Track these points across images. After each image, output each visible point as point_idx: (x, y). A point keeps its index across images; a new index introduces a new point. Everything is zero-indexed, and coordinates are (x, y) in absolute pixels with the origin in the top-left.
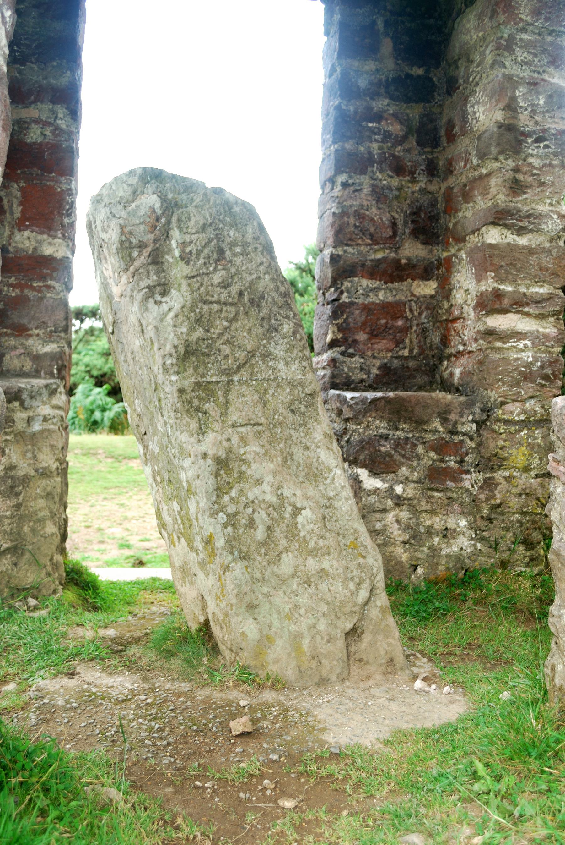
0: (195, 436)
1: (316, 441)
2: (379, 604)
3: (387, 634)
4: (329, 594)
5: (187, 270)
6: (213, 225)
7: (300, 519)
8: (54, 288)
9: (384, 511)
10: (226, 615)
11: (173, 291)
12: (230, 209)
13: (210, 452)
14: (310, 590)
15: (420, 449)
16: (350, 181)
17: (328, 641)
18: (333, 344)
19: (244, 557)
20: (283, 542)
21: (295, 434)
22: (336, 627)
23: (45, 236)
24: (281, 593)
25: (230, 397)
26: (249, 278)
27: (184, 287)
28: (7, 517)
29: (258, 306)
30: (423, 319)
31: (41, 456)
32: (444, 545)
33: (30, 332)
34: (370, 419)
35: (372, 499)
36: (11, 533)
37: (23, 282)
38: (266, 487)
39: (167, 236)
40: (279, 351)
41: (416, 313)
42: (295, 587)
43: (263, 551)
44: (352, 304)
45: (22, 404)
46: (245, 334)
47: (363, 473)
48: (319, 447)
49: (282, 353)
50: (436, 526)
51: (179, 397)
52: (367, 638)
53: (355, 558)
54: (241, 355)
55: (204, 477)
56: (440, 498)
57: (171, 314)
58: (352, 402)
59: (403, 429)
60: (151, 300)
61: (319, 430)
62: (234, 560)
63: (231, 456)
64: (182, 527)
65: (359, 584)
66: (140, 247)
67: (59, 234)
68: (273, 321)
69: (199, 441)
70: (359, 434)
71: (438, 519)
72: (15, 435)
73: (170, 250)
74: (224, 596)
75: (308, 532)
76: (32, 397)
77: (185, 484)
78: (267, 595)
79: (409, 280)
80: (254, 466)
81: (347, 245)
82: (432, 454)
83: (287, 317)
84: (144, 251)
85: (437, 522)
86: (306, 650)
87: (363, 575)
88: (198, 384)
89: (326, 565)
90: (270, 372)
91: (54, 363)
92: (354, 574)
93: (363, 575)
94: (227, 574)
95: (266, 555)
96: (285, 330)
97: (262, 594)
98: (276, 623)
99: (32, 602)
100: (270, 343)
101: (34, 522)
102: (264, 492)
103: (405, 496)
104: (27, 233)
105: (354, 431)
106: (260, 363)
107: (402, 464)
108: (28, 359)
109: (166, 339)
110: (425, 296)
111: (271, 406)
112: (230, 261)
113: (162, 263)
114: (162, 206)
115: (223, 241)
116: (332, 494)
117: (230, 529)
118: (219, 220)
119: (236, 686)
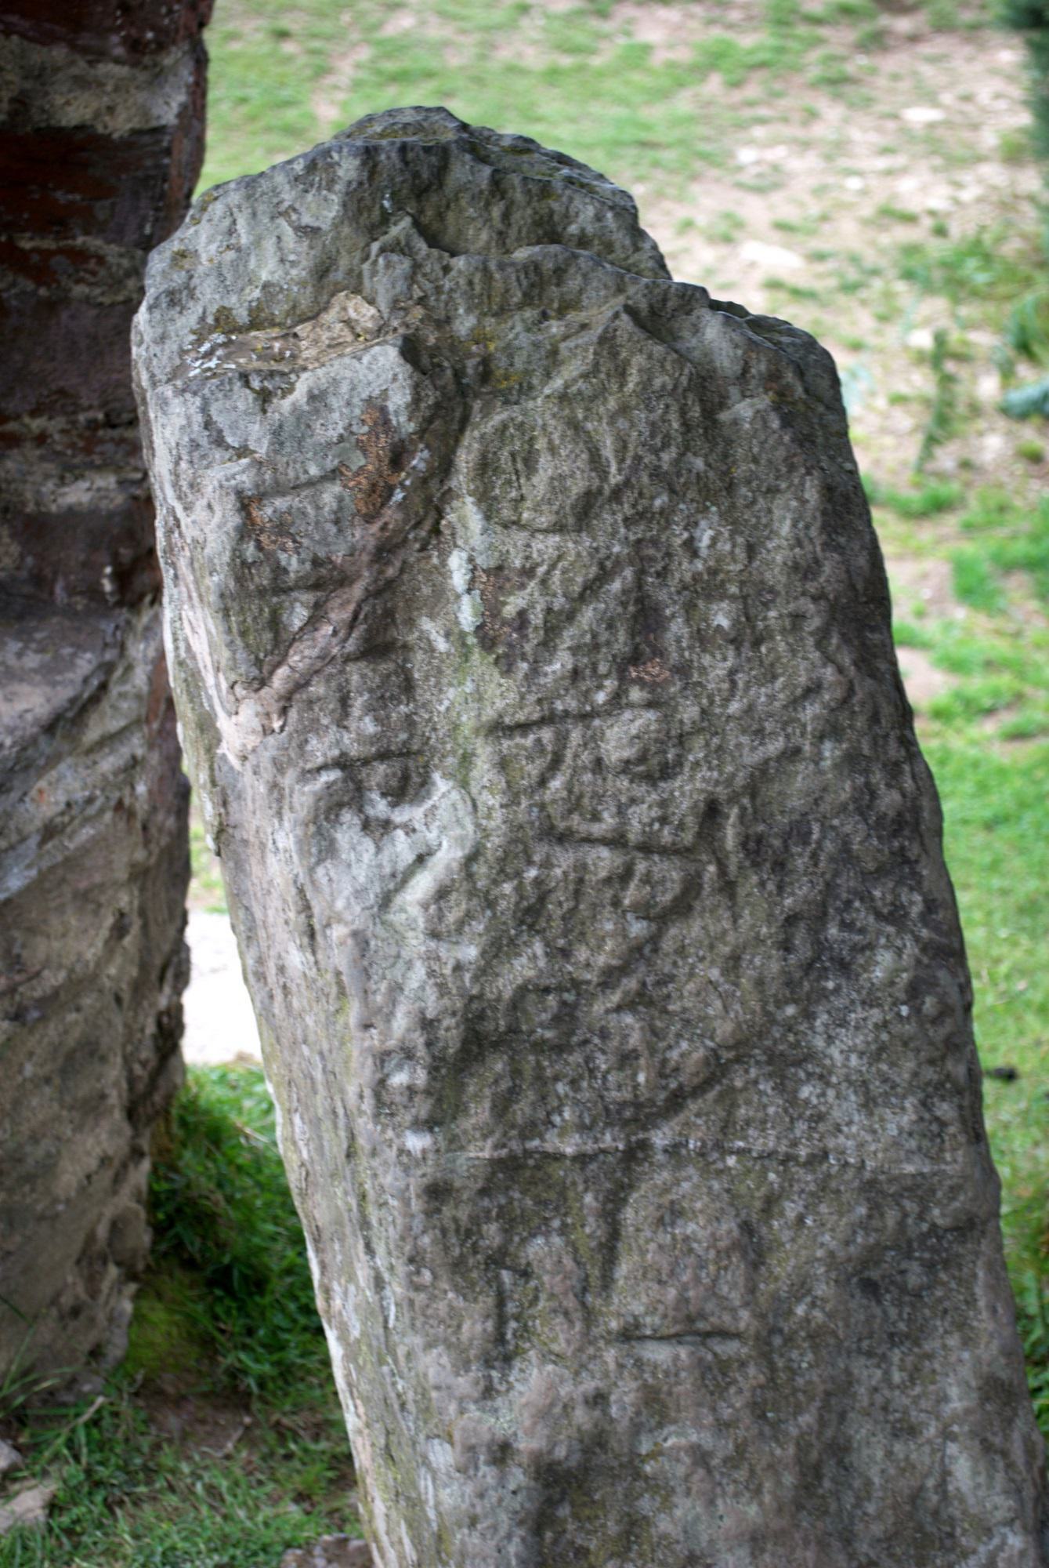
5: (501, 694)
6: (629, 497)
8: (101, 260)
11: (441, 785)
12: (709, 414)
13: (525, 1445)
21: (867, 1373)
23: (59, 53)
25: (629, 1215)
26: (752, 758)
27: (483, 770)
29: (780, 866)
33: (12, 426)
39: (436, 531)
40: (843, 1051)
46: (715, 974)
49: (854, 1060)
51: (428, 1214)
54: (688, 1054)
55: (495, 1528)
57: (423, 885)
61: (965, 1372)
66: (317, 586)
67: (116, 45)
68: (833, 931)
83: (896, 916)
84: (335, 603)
90: (801, 1127)
91: (103, 556)
96: (879, 974)
100: (809, 1016)
106: (765, 1086)
109: (397, 988)
111: (783, 1268)
112: (683, 670)
113: (406, 647)
114: (417, 400)
118: (656, 474)
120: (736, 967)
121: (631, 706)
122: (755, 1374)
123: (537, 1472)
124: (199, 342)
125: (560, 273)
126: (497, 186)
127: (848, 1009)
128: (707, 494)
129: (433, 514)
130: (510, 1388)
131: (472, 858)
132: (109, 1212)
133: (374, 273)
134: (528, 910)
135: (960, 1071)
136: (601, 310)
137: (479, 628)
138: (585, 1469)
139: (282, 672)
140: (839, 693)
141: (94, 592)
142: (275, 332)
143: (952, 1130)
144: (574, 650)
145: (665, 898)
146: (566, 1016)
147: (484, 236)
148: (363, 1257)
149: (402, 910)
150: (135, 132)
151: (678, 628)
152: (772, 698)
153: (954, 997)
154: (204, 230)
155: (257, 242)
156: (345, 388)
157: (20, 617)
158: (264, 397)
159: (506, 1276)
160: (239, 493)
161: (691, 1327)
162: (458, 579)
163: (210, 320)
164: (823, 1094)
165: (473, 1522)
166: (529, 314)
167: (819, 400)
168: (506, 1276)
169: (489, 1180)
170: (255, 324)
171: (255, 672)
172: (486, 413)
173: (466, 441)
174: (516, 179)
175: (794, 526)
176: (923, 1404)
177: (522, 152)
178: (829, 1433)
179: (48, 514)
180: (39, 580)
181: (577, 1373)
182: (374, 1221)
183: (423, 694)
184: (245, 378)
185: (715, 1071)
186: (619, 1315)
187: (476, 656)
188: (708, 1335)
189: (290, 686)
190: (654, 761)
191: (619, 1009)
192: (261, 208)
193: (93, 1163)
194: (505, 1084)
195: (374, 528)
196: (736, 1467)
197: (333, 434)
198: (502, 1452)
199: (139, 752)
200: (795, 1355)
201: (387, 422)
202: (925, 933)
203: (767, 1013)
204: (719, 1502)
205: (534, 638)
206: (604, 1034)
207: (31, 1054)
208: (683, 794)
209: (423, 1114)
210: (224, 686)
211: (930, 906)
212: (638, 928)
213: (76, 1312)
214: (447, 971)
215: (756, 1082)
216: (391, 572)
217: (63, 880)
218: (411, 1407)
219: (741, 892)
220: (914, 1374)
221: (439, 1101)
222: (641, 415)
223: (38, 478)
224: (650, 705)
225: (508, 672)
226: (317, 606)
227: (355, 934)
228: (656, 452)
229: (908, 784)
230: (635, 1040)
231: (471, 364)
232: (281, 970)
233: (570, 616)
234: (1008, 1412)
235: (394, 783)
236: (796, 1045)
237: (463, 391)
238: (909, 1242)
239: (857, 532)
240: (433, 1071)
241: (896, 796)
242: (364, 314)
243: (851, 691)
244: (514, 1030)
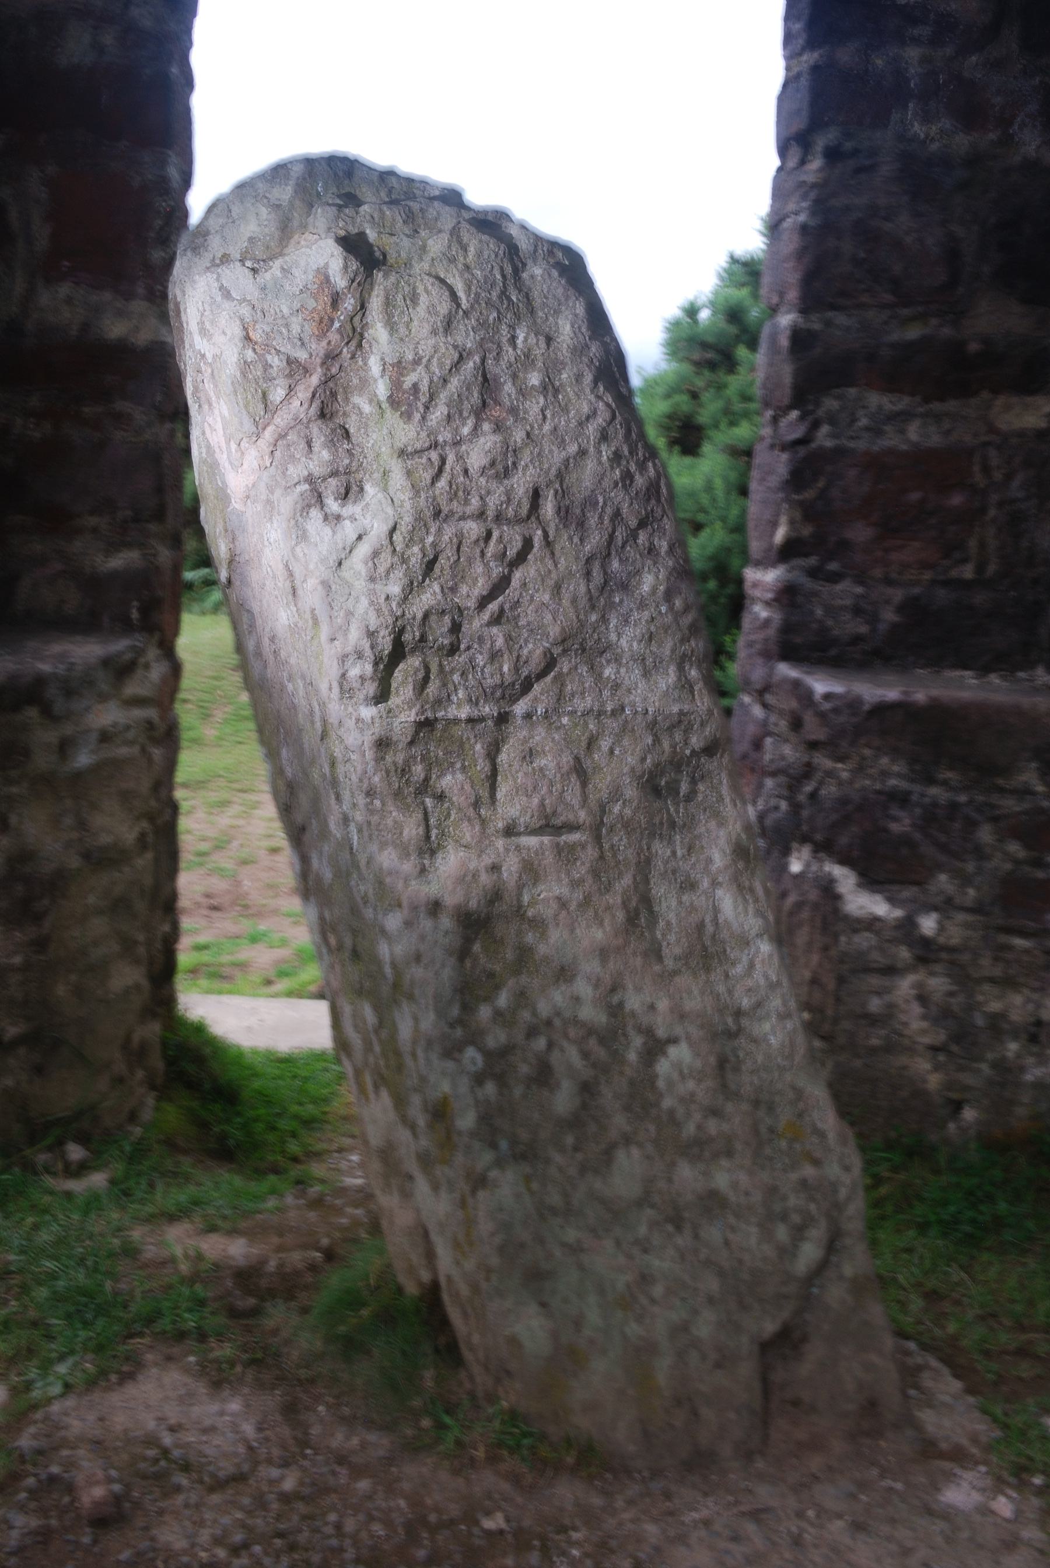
2: (848, 1270)
5: (407, 433)
6: (474, 315)
7: (663, 1067)
9: (891, 971)
10: (475, 1289)
11: (370, 489)
12: (516, 272)
14: (679, 1241)
15: (985, 834)
16: (848, 145)
17: (718, 1365)
18: (787, 552)
19: (525, 1154)
20: (620, 1122)
21: (659, 848)
23: (107, 296)
24: (608, 1244)
25: (503, 758)
27: (398, 479)
29: (581, 524)
30: (1016, 489)
31: (99, 821)
32: (1030, 1060)
34: (867, 752)
35: (864, 940)
38: (583, 988)
40: (627, 640)
41: (998, 476)
42: (643, 1230)
43: (570, 1140)
44: (839, 452)
45: (47, 712)
46: (546, 597)
47: (844, 878)
50: (1015, 1016)
52: (815, 1352)
54: (534, 651)
56: (1027, 951)
57: (364, 549)
58: (827, 706)
59: (945, 783)
60: (315, 513)
62: (499, 1163)
64: (382, 1063)
67: (141, 290)
70: (841, 783)
71: (1018, 999)
73: (365, 383)
77: (388, 970)
78: (575, 1249)
79: (985, 395)
80: (555, 935)
81: (833, 307)
82: (1014, 848)
84: (300, 388)
85: (1017, 1005)
87: (812, 1207)
88: (425, 725)
89: (721, 1180)
90: (606, 693)
93: (812, 1207)
95: (576, 1149)
96: (646, 588)
98: (594, 1317)
99: (75, 1152)
100: (604, 619)
103: (942, 940)
104: (64, 289)
105: (830, 774)
107: (940, 867)
109: (350, 614)
110: (1021, 434)
111: (601, 784)
112: (513, 411)
114: (346, 267)
115: (498, 358)
116: (746, 1003)
117: (490, 1088)
119: (493, 1459)
122: (591, 853)
123: (459, 916)
129: (357, 336)
139: (270, 429)
145: (511, 553)
146: (456, 628)
151: (508, 388)
152: (568, 421)
159: (429, 802)
161: (548, 825)
164: (618, 672)
168: (429, 802)
175: (572, 326)
181: (479, 856)
185: (550, 663)
187: (388, 412)
189: (276, 436)
198: (435, 907)
204: (578, 931)
208: (519, 485)
214: (382, 600)
215: (576, 668)
219: (557, 547)
220: (690, 849)
230: (500, 642)
235: (342, 491)
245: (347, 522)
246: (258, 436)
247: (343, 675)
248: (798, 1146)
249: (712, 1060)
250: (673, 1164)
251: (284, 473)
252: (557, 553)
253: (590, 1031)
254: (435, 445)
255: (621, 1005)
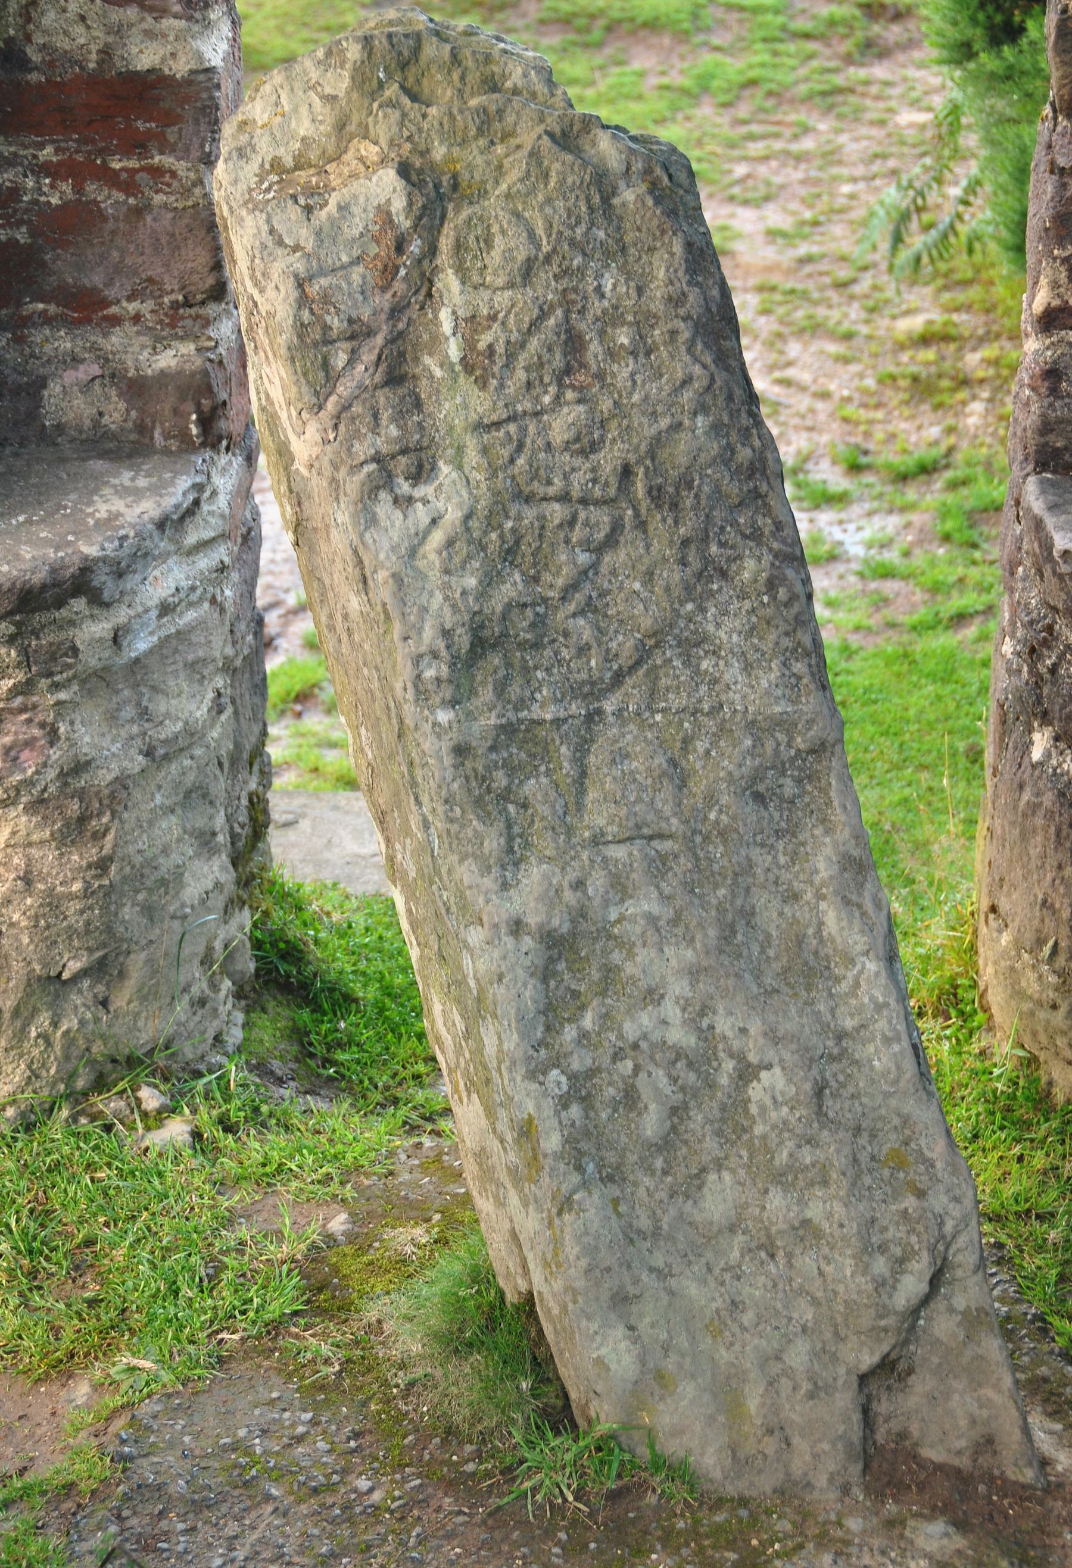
0: (496, 871)
1: (817, 880)
2: (960, 1302)
3: (976, 1374)
4: (818, 1282)
5: (481, 403)
6: (556, 260)
7: (755, 1092)
8: (174, 174)
10: (564, 1308)
11: (444, 469)
12: (606, 200)
13: (532, 920)
17: (811, 1396)
19: (612, 1177)
20: (711, 1144)
21: (762, 859)
22: (834, 1358)
27: (472, 456)
28: (71, 897)
29: (674, 506)
31: (161, 706)
33: (114, 310)
36: (88, 932)
37: (80, 158)
38: (671, 1010)
39: (429, 295)
40: (727, 632)
42: (736, 1254)
43: (659, 1163)
46: (637, 586)
48: (823, 897)
49: (735, 638)
51: (455, 767)
52: (921, 1384)
53: (896, 1196)
54: (624, 644)
57: (437, 537)
61: (828, 850)
62: (585, 1185)
63: (584, 926)
65: (902, 1261)
66: (352, 338)
68: (714, 549)
69: (505, 886)
72: (83, 682)
73: (436, 341)
74: (559, 1265)
75: (774, 1127)
76: (120, 575)
77: (472, 983)
78: (662, 1274)
80: (642, 955)
83: (755, 536)
84: (365, 349)
86: (753, 1410)
88: (508, 730)
89: (814, 1211)
91: (190, 406)
92: (890, 1234)
93: (914, 1239)
94: (566, 1217)
95: (665, 1173)
96: (746, 575)
97: (651, 1270)
99: (151, 1098)
100: (703, 610)
101: (150, 890)
102: (665, 1022)
108: (113, 392)
111: (698, 787)
112: (600, 376)
114: (410, 204)
115: (582, 312)
116: (849, 1023)
117: (575, 1111)
118: (572, 243)
120: (651, 580)
121: (567, 403)
124: (261, 182)
125: (500, 112)
126: (455, 57)
127: (728, 603)
128: (608, 254)
130: (519, 882)
131: (468, 517)
132: (222, 935)
133: (376, 123)
134: (509, 551)
135: (807, 640)
136: (528, 135)
137: (463, 359)
138: (573, 934)
139: (333, 399)
140: (705, 382)
141: (184, 436)
142: (312, 171)
143: (805, 681)
144: (527, 369)
145: (600, 536)
146: (539, 623)
147: (449, 93)
148: (414, 808)
149: (425, 557)
150: (192, 72)
151: (595, 347)
152: (660, 389)
153: (799, 588)
154: (259, 104)
155: (295, 110)
156: (362, 200)
157: (130, 456)
158: (309, 210)
159: (511, 808)
160: (296, 276)
162: (447, 327)
163: (267, 166)
165: (500, 978)
166: (482, 142)
167: (680, 186)
168: (511, 808)
169: (495, 740)
170: (298, 167)
171: (314, 400)
172: (457, 210)
173: (445, 231)
174: (467, 52)
176: (801, 877)
177: (471, 34)
178: (739, 902)
179: (146, 377)
180: (143, 429)
182: (420, 780)
183: (428, 408)
184: (294, 198)
186: (589, 827)
187: (462, 379)
188: (651, 838)
190: (585, 441)
191: (574, 615)
192: (296, 85)
193: (210, 886)
194: (502, 673)
195: (388, 296)
196: (676, 926)
197: (356, 233)
199: (227, 560)
200: (711, 848)
201: (391, 221)
202: (775, 545)
203: (674, 610)
205: (500, 362)
206: (566, 634)
207: (160, 787)
209: (448, 696)
210: (294, 414)
211: (778, 526)
212: (583, 558)
213: (202, 1002)
214: (457, 595)
215: (671, 660)
216: (401, 326)
217: (176, 651)
218: (454, 909)
219: (651, 528)
220: (794, 857)
221: (458, 686)
222: (560, 204)
223: (136, 349)
224: (579, 401)
225: (484, 387)
226: (353, 351)
227: (393, 575)
228: (572, 228)
229: (757, 443)
230: (587, 635)
231: (445, 180)
232: (346, 617)
233: (523, 345)
234: (860, 878)
235: (413, 470)
236: (695, 632)
237: (441, 197)
238: (783, 764)
239: (711, 274)
240: (452, 665)
241: (748, 452)
242: (371, 151)
243: (712, 379)
244: (504, 635)
245: (419, 505)
246: (320, 408)
247: (419, 676)
248: (902, 1175)
249: (808, 1086)
250: (766, 1191)
251: (349, 450)
252: (651, 533)
253: (679, 1054)
254: (512, 418)
255: (712, 1027)
